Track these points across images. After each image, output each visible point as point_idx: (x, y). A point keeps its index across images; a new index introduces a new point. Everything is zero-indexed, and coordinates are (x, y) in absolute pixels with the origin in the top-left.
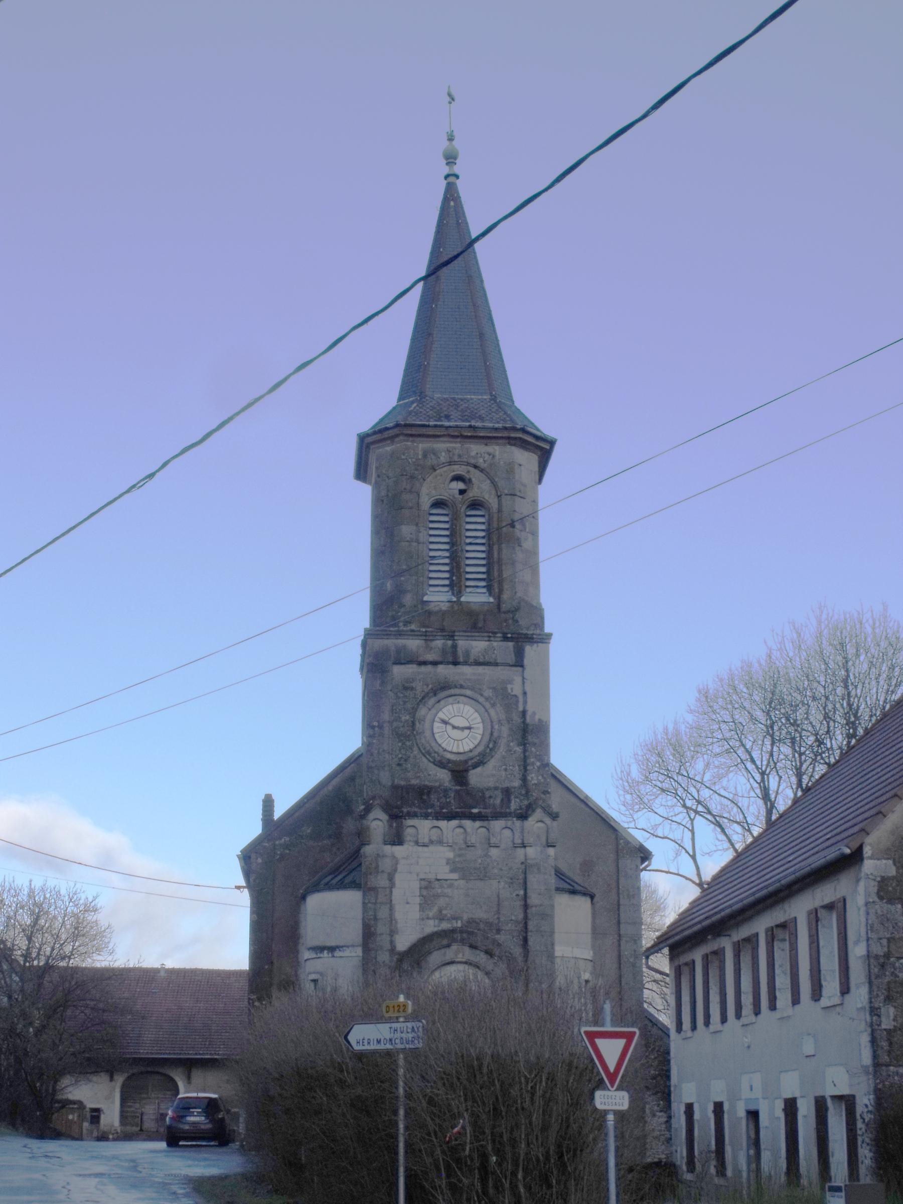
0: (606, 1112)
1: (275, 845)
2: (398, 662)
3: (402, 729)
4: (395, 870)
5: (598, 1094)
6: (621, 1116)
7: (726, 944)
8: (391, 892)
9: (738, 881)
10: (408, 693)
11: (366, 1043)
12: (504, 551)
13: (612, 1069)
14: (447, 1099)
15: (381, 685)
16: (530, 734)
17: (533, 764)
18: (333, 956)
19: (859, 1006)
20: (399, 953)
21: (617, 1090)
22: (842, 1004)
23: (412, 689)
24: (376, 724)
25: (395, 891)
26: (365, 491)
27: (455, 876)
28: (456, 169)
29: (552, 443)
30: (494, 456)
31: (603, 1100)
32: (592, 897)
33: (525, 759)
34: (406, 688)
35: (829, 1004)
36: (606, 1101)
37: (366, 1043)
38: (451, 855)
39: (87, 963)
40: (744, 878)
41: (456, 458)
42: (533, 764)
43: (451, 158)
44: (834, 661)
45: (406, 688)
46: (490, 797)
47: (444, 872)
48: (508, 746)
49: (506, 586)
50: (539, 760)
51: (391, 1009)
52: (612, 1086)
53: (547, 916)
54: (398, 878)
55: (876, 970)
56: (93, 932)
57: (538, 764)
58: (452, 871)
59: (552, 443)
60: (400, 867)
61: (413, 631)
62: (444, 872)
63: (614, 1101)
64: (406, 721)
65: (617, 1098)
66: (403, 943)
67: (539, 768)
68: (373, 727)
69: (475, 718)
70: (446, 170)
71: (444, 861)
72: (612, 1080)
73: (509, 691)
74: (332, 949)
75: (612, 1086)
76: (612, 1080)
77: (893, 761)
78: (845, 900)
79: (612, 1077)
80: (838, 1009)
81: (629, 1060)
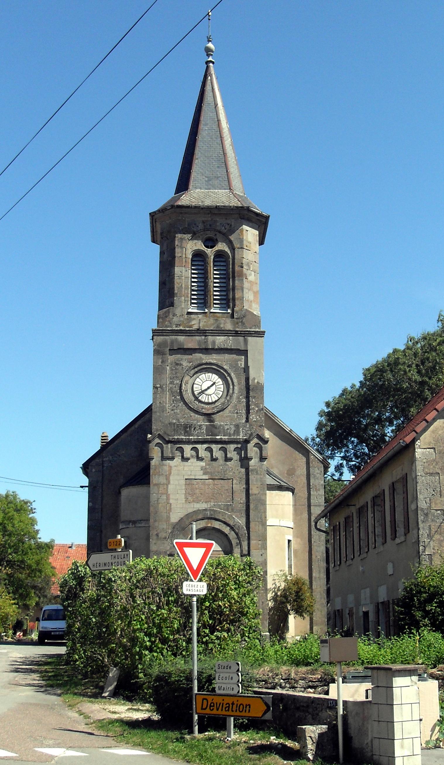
0: (192, 596)
1: (103, 461)
3: (174, 389)
4: (170, 474)
5: (185, 584)
6: (201, 600)
7: (353, 510)
8: (167, 488)
10: (178, 367)
11: (98, 566)
12: (236, 282)
13: (195, 567)
15: (161, 363)
16: (251, 391)
17: (253, 409)
18: (135, 527)
19: (414, 541)
20: (172, 524)
21: (198, 581)
22: (405, 541)
23: (181, 364)
24: (158, 386)
25: (170, 487)
26: (157, 248)
29: (267, 218)
30: (231, 225)
31: (189, 588)
32: (292, 491)
34: (177, 364)
35: (399, 542)
36: (191, 588)
37: (98, 566)
41: (208, 227)
42: (253, 409)
45: (177, 364)
46: (228, 429)
47: (200, 475)
48: (239, 398)
49: (237, 302)
50: (257, 407)
51: (112, 543)
52: (195, 579)
53: (263, 503)
54: (171, 478)
55: (422, 517)
56: (303, 597)
57: (257, 409)
58: (204, 474)
59: (267, 218)
61: (181, 330)
62: (200, 475)
63: (196, 589)
64: (177, 384)
65: (199, 587)
66: (175, 518)
67: (257, 411)
68: (157, 388)
69: (219, 382)
71: (199, 468)
72: (195, 575)
73: (240, 365)
74: (134, 522)
75: (195, 579)
76: (195, 575)
78: (407, 474)
79: (195, 573)
80: (404, 543)
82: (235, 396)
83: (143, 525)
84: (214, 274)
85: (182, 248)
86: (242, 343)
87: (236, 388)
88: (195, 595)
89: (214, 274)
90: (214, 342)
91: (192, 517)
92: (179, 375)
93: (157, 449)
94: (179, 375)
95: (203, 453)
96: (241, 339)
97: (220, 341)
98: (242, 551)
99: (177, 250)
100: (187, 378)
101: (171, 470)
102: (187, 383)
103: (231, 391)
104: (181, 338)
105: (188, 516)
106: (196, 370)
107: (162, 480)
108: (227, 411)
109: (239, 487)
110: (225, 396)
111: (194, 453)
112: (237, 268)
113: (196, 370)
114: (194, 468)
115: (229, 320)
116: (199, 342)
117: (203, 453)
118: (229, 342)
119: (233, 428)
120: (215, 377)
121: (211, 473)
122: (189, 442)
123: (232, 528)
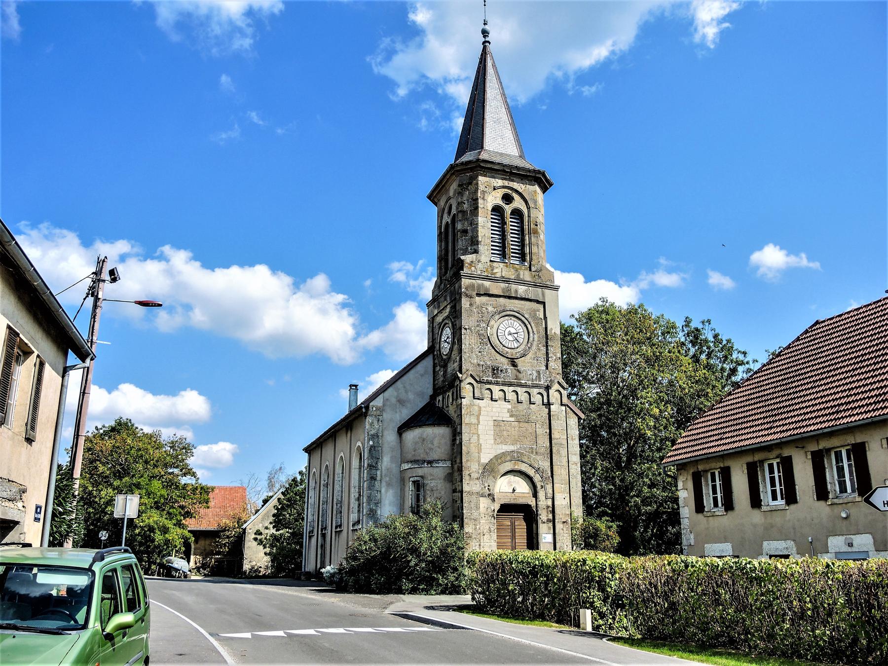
2: (479, 295)
4: (480, 414)
9: (738, 416)
14: (164, 510)
27: (512, 419)
28: (487, 27)
33: (547, 354)
38: (510, 407)
39: (19, 239)
40: (712, 439)
43: (485, 33)
44: (630, 447)
47: (506, 416)
58: (511, 416)
60: (482, 413)
62: (506, 416)
66: (485, 460)
70: (483, 26)
71: (506, 411)
77: (740, 410)
81: (388, 632)
82: (535, 343)
83: (440, 465)
84: (511, 225)
85: (483, 199)
86: (540, 295)
87: (536, 336)
88: (301, 547)
89: (511, 225)
90: (516, 291)
91: (500, 458)
92: (484, 319)
93: (469, 387)
94: (484, 319)
95: (511, 396)
96: (539, 290)
97: (522, 290)
98: (546, 494)
99: (480, 201)
100: (492, 323)
101: (480, 411)
102: (492, 327)
103: (531, 339)
104: (487, 284)
105: (497, 457)
106: (501, 315)
107: (474, 420)
108: (528, 357)
109: (542, 431)
110: (525, 343)
111: (502, 393)
112: (533, 226)
113: (501, 315)
114: (501, 410)
115: (527, 273)
116: (503, 290)
117: (511, 396)
118: (532, 293)
119: (535, 374)
120: (517, 324)
121: (516, 416)
122: (497, 383)
123: (537, 470)
